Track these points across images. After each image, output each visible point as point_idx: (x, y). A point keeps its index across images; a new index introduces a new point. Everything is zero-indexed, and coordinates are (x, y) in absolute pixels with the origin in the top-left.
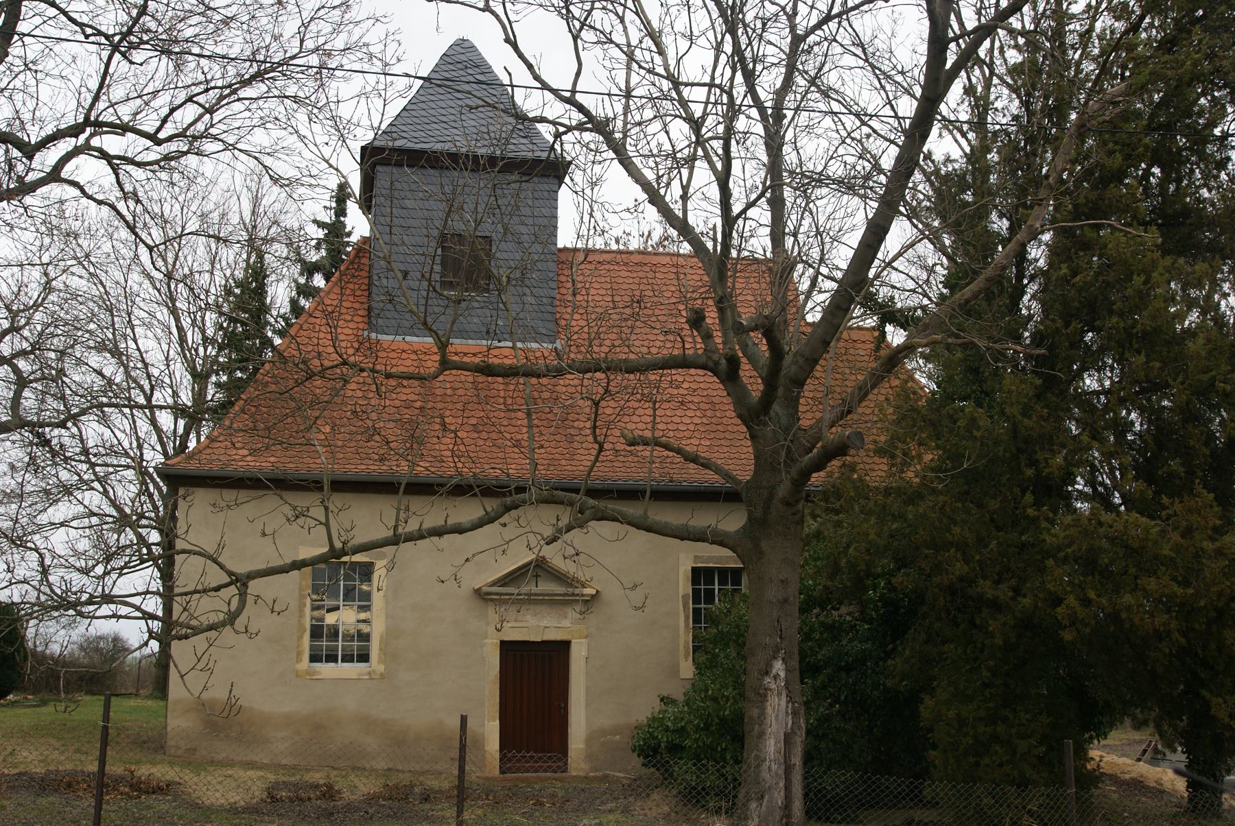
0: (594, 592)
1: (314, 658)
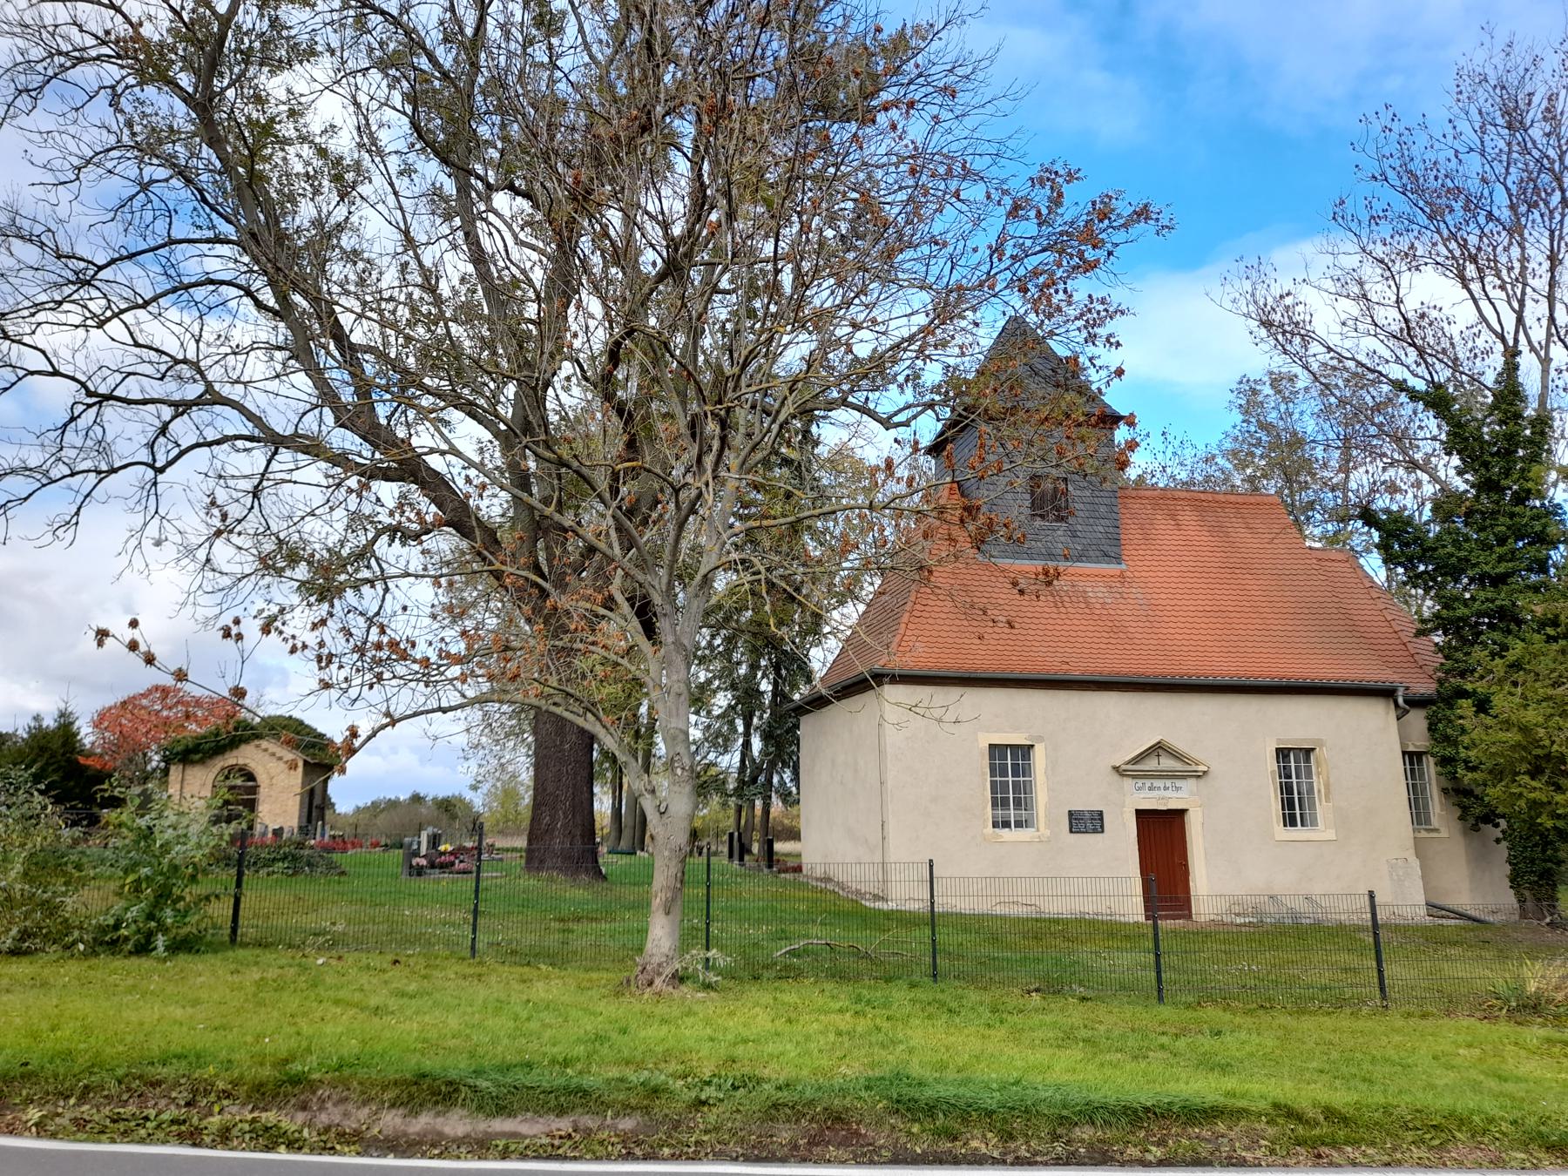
0: (1205, 769)
1: (995, 825)
